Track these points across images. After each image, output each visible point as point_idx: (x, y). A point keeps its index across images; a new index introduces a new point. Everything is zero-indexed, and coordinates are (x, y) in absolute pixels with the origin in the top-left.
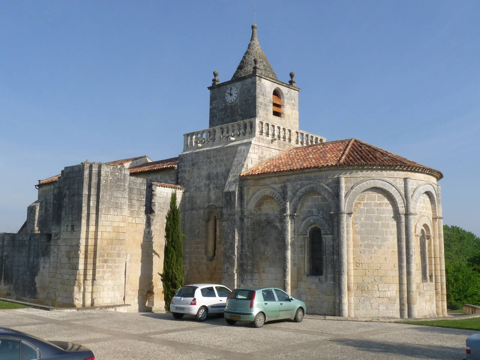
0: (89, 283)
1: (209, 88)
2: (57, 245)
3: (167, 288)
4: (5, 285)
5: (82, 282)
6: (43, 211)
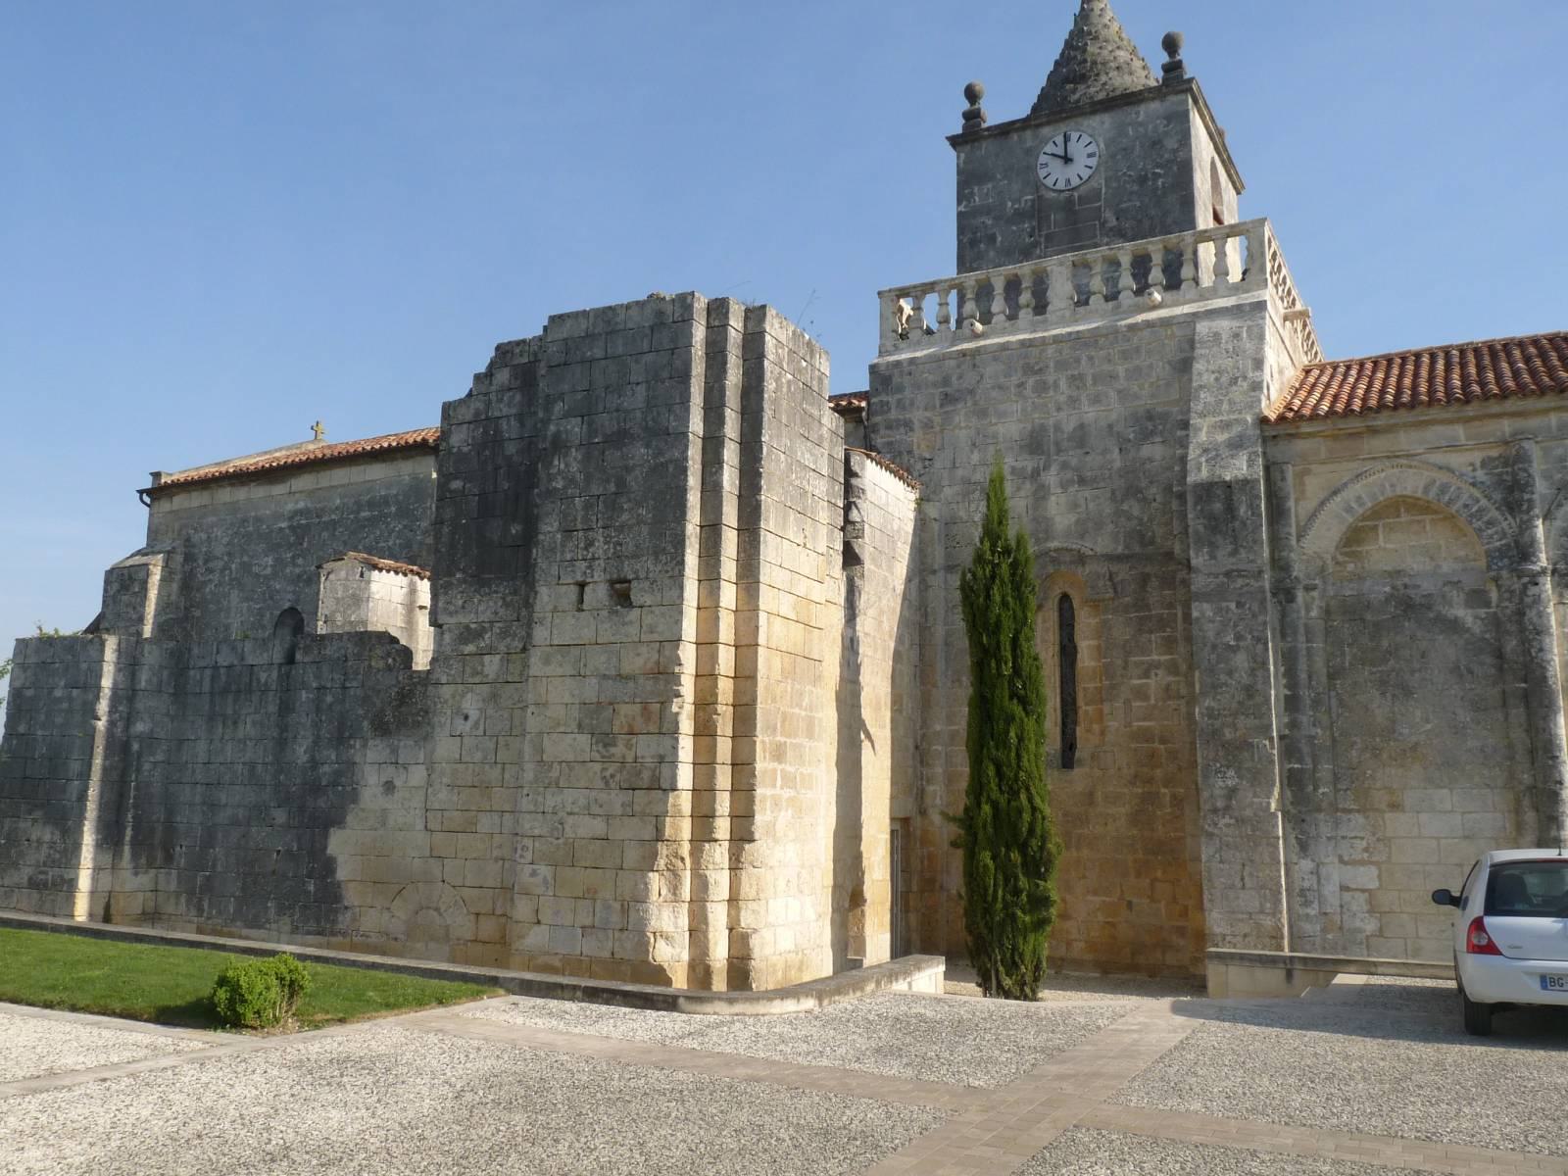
0: (719, 854)
1: (955, 141)
2: (477, 679)
3: (1000, 877)
4: (136, 874)
5: (685, 850)
6: (175, 586)
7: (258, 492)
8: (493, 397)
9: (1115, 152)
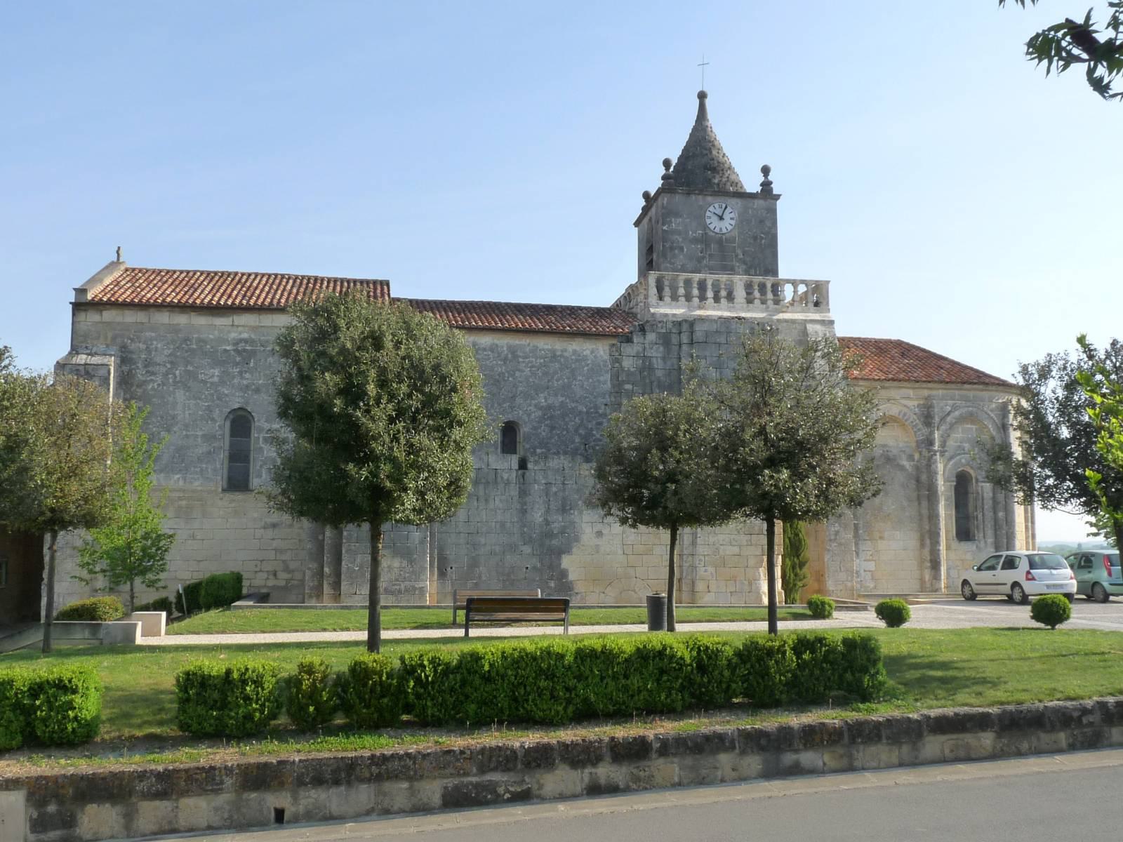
7: (201, 321)
8: (647, 346)
9: (743, 221)
